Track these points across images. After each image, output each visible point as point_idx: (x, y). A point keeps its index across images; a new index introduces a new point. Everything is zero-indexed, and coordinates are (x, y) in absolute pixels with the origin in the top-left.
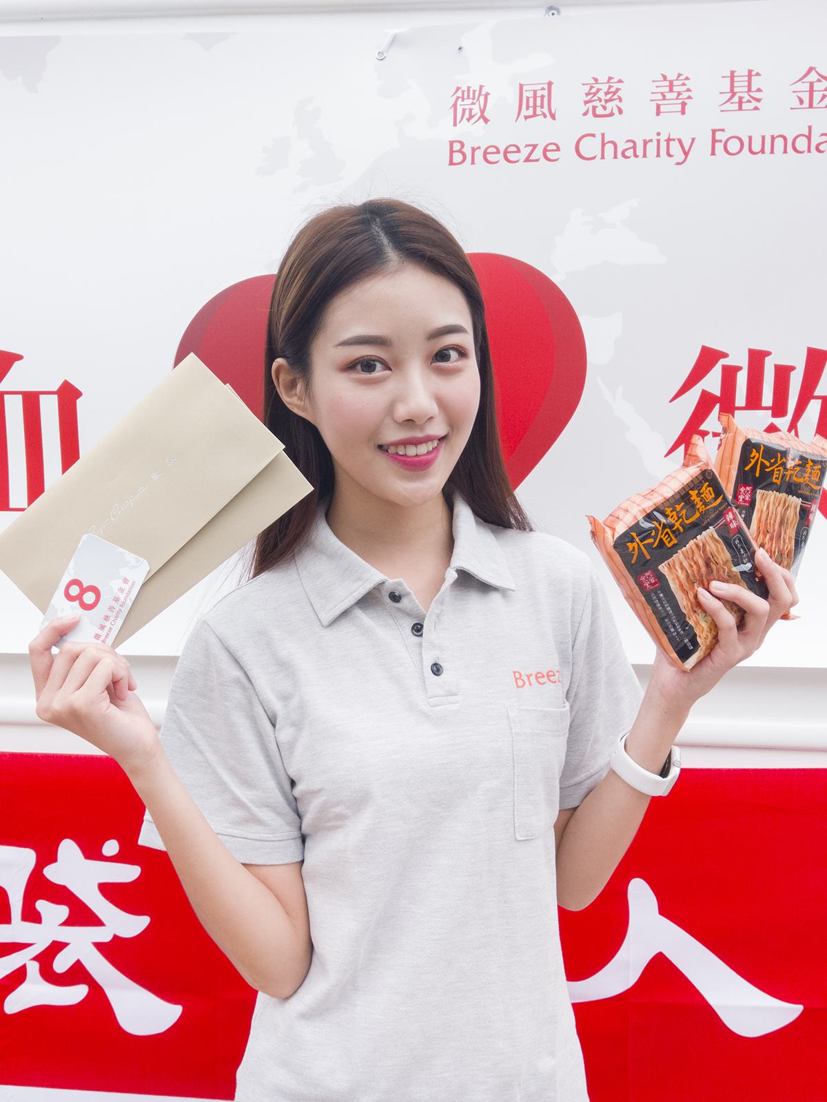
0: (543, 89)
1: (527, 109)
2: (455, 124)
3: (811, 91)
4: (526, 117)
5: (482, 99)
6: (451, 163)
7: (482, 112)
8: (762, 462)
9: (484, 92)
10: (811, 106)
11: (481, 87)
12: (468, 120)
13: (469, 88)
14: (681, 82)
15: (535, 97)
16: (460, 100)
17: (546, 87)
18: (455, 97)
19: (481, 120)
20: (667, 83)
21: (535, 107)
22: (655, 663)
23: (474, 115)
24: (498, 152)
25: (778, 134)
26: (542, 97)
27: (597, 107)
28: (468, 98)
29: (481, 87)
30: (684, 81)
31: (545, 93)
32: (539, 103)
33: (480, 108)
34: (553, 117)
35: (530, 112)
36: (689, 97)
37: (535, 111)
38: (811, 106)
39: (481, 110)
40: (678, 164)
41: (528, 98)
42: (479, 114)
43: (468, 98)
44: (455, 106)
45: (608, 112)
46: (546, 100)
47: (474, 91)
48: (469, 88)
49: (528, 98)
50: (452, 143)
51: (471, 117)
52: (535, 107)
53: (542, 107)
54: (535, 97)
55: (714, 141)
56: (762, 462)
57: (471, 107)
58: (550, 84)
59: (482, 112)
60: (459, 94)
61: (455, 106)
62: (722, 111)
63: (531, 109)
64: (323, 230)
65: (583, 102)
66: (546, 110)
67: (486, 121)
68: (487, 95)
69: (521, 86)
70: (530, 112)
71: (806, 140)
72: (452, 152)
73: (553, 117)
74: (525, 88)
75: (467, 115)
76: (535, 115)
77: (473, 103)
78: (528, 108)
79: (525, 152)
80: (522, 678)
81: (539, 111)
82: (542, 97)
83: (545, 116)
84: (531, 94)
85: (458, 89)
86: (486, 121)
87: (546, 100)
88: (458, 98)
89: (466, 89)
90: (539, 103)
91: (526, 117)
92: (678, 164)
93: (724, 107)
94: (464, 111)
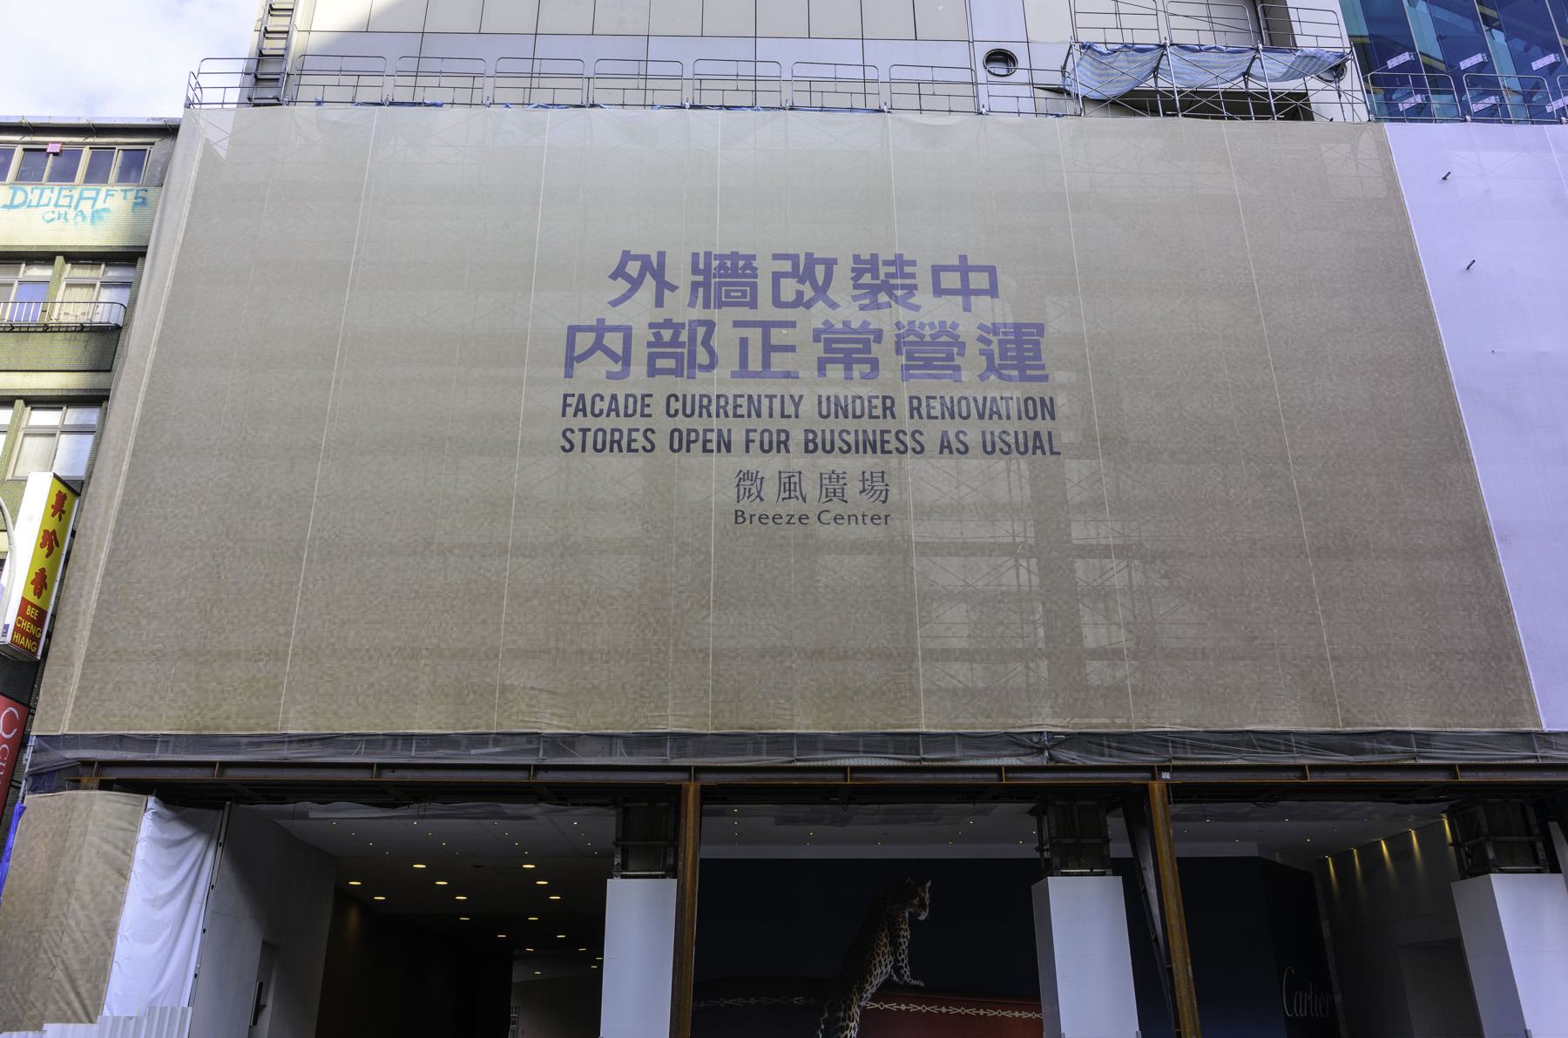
1: (785, 492)
2: (738, 502)
4: (784, 499)
5: (759, 481)
6: (736, 523)
7: (759, 492)
8: (875, 998)
9: (759, 476)
11: (757, 472)
13: (748, 471)
21: (790, 490)
22: (770, 331)
24: (768, 518)
26: (795, 483)
29: (757, 472)
36: (845, 484)
37: (790, 480)
41: (785, 483)
42: (756, 494)
43: (748, 479)
46: (798, 485)
47: (752, 474)
49: (785, 483)
50: (736, 511)
51: (750, 496)
53: (795, 491)
56: (875, 998)
59: (759, 492)
60: (741, 476)
61: (738, 485)
64: (685, 843)
65: (797, 350)
66: (798, 494)
68: (762, 478)
70: (787, 495)
72: (737, 516)
76: (790, 498)
77: (752, 485)
79: (786, 519)
82: (795, 483)
83: (798, 499)
85: (741, 471)
86: (762, 500)
87: (798, 485)
88: (740, 479)
91: (784, 499)
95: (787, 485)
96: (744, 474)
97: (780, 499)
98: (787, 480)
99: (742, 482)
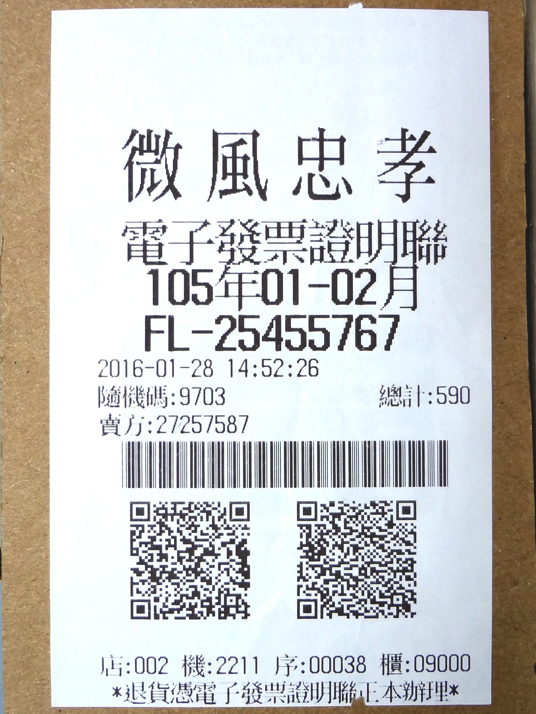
1: (224, 178)
2: (130, 199)
4: (223, 193)
5: (170, 153)
7: (171, 179)
9: (172, 143)
11: (168, 134)
12: (150, 190)
13: (149, 132)
16: (137, 152)
18: (129, 149)
19: (170, 192)
21: (235, 174)
23: (159, 183)
25: (213, 369)
26: (245, 158)
27: (314, 175)
28: (149, 150)
29: (168, 134)
32: (240, 169)
33: (167, 171)
34: (263, 194)
35: (228, 184)
39: (169, 177)
41: (225, 159)
42: (165, 183)
45: (331, 191)
46: (250, 164)
47: (158, 137)
48: (149, 132)
51: (153, 186)
55: (148, 331)
57: (154, 166)
58: (255, 134)
59: (171, 179)
60: (135, 142)
61: (130, 164)
62: (382, 182)
66: (251, 181)
67: (177, 195)
69: (215, 135)
73: (263, 194)
75: (148, 183)
76: (234, 190)
78: (225, 175)
82: (245, 158)
87: (250, 164)
88: (134, 149)
89: (145, 134)
90: (240, 169)
91: (223, 193)
93: (382, 178)
94: (143, 171)
95: (230, 162)
96: (142, 137)
97: (216, 193)
98: (228, 152)
99: (137, 157)
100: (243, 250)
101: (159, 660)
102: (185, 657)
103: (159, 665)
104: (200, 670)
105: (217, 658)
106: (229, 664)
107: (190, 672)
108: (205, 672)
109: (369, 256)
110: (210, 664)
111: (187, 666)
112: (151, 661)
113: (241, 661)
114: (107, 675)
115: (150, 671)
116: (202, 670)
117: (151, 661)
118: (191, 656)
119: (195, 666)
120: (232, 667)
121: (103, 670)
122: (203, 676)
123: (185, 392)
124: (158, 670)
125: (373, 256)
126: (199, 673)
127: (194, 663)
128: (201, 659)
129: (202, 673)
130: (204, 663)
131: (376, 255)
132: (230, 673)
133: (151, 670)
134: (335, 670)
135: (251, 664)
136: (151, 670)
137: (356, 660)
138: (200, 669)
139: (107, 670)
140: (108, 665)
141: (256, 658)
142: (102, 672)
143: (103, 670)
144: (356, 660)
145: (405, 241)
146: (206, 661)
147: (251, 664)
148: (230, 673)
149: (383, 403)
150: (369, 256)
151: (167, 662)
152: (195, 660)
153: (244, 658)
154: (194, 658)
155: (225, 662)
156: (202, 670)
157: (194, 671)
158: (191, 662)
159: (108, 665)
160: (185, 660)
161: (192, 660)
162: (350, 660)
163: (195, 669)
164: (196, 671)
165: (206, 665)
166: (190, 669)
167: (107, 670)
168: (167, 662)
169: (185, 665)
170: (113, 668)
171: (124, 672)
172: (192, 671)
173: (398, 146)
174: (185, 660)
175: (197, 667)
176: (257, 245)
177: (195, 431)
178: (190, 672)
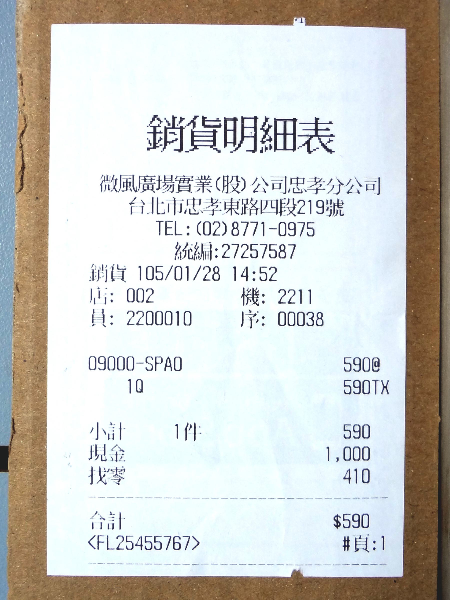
0: (130, 178)
3: (116, 455)
4: (123, 191)
5: (114, 181)
10: (116, 461)
11: (113, 176)
14: (207, 183)
15: (127, 182)
17: (132, 177)
20: (202, 183)
21: (127, 186)
26: (130, 183)
29: (113, 176)
30: (208, 183)
31: (131, 180)
38: (116, 461)
40: (317, 212)
41: (124, 183)
44: (101, 185)
52: (127, 186)
54: (127, 182)
63: (125, 187)
71: (157, 362)
74: (122, 177)
78: (124, 186)
80: (213, 273)
81: (129, 188)
82: (130, 183)
84: (125, 181)
91: (123, 191)
92: (317, 212)
100: (233, 185)
101: (147, 291)
102: (244, 289)
103: (147, 295)
104: (255, 301)
105: (279, 290)
106: (289, 295)
107: (248, 302)
108: (260, 302)
109: (234, 146)
110: (263, 295)
111: (245, 297)
112: (140, 292)
113: (298, 293)
114: (95, 303)
115: (139, 300)
116: (257, 300)
117: (140, 292)
118: (248, 288)
119: (252, 296)
120: (281, 298)
121: (91, 299)
122: (258, 305)
123: (292, 226)
124: (146, 299)
125: (237, 146)
126: (255, 303)
127: (251, 294)
128: (257, 291)
129: (257, 303)
130: (259, 294)
131: (240, 145)
132: (289, 302)
133: (140, 299)
134: (345, 458)
135: (306, 295)
136: (140, 299)
137: (315, 315)
138: (255, 300)
139: (94, 299)
140: (95, 295)
141: (310, 291)
142: (91, 301)
143: (91, 299)
144: (315, 315)
145: (235, 130)
146: (261, 293)
147: (306, 295)
148: (289, 302)
149: (266, 149)
150: (234, 146)
151: (153, 293)
152: (251, 292)
153: (301, 291)
154: (250, 290)
155: (285, 294)
156: (257, 300)
157: (251, 301)
158: (248, 293)
159: (95, 295)
160: (244, 292)
161: (249, 292)
162: (310, 315)
163: (251, 299)
164: (252, 301)
165: (260, 296)
166: (248, 299)
167: (94, 299)
168: (153, 293)
169: (243, 296)
170: (99, 298)
171: (108, 301)
172: (249, 301)
173: (314, 180)
174: (244, 292)
175: (253, 298)
176: (239, 183)
177: (310, 235)
178: (248, 302)
